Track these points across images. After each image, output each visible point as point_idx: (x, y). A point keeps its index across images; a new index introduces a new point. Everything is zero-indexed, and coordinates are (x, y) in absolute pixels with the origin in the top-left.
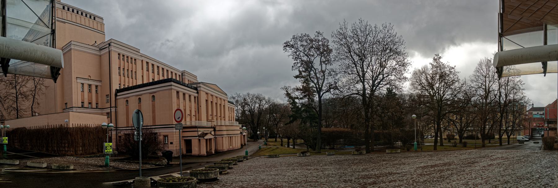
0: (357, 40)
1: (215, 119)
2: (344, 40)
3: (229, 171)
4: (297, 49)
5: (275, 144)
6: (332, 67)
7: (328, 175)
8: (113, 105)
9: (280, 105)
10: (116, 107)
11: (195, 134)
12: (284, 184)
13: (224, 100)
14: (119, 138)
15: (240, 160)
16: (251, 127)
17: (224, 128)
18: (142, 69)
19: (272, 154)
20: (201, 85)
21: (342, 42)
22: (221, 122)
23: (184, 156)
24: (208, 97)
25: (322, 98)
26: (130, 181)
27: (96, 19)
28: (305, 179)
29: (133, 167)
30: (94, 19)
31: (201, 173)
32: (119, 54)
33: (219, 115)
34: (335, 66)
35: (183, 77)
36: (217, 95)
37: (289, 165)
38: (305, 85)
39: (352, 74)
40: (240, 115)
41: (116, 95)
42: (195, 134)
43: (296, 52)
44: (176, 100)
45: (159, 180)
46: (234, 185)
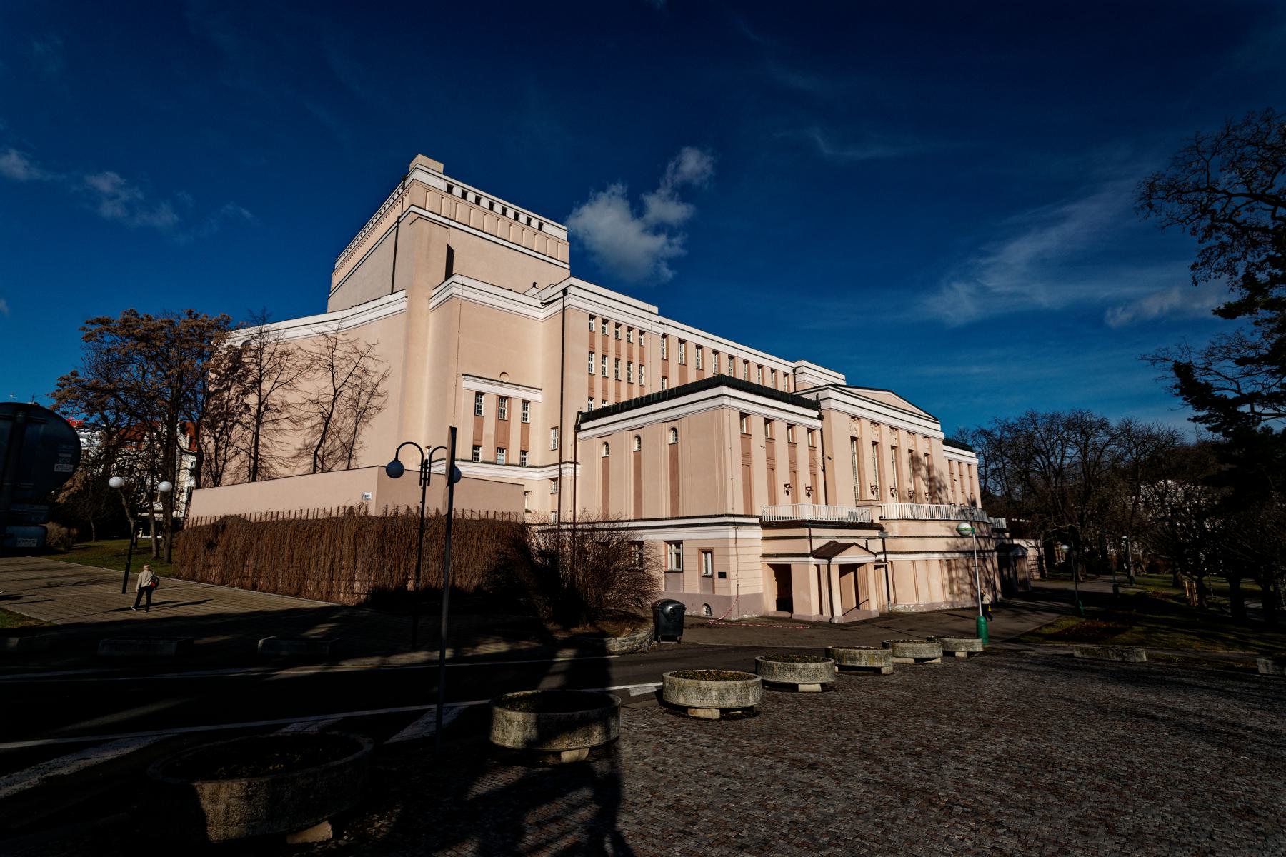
8: (568, 456)
20: (831, 393)
30: (540, 226)
41: (577, 429)
42: (804, 547)
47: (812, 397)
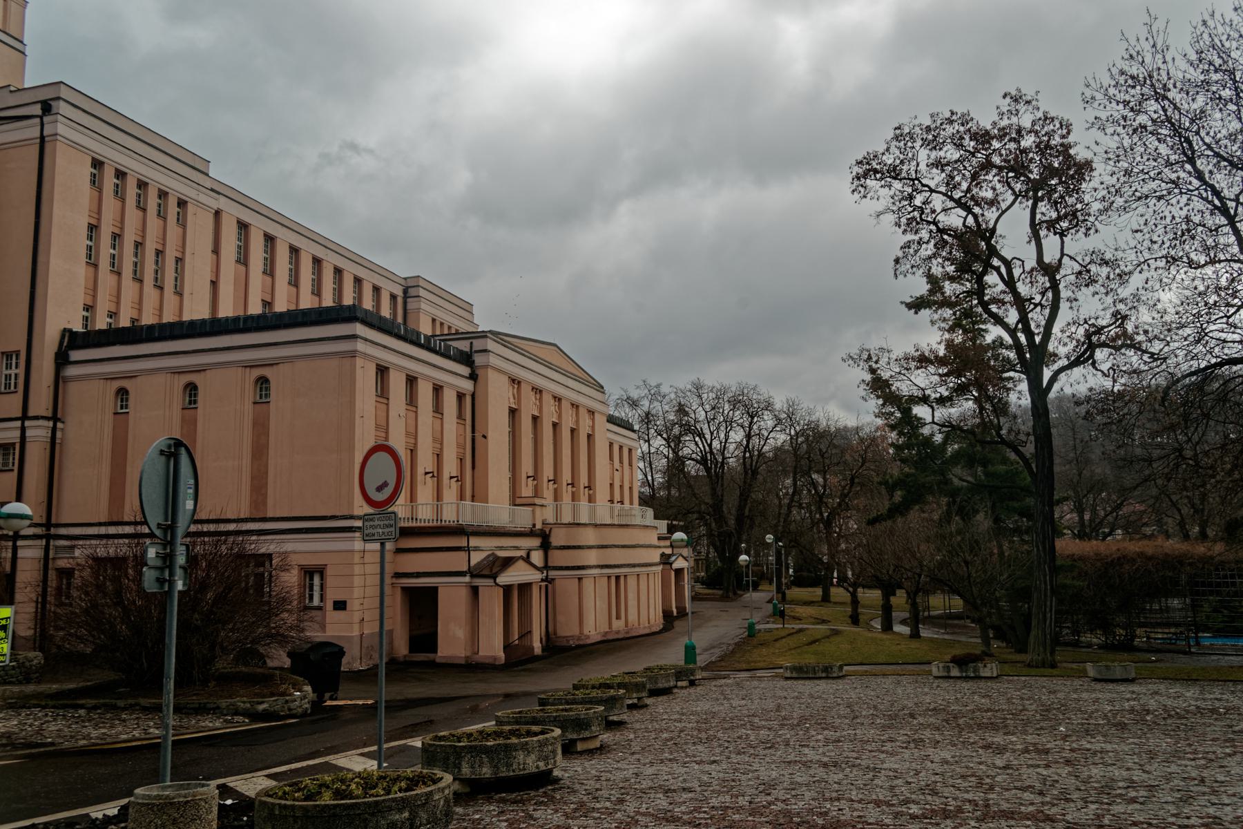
0: (1226, 93)
1: (548, 493)
2: (1152, 106)
3: (606, 737)
4: (914, 180)
5: (823, 612)
6: (1093, 242)
7: (1107, 787)
9: (843, 432)
10: (55, 418)
11: (457, 561)
12: (872, 814)
13: (591, 412)
14: (57, 582)
15: (662, 684)
16: (710, 535)
17: (590, 537)
18: (216, 251)
19: (809, 659)
20: (491, 345)
21: (1142, 119)
22: (575, 511)
23: (397, 669)
24: (518, 397)
25: (1052, 395)
26: (97, 812)
28: (978, 796)
29: (128, 730)
31: (476, 751)
32: (97, 164)
33: (566, 476)
34: (1113, 235)
35: (412, 304)
36: (560, 391)
37: (894, 719)
38: (958, 338)
39: (1213, 262)
40: (659, 479)
41: (62, 359)
42: (457, 561)
43: (911, 197)
44: (371, 403)
45: (267, 793)
46: (631, 807)
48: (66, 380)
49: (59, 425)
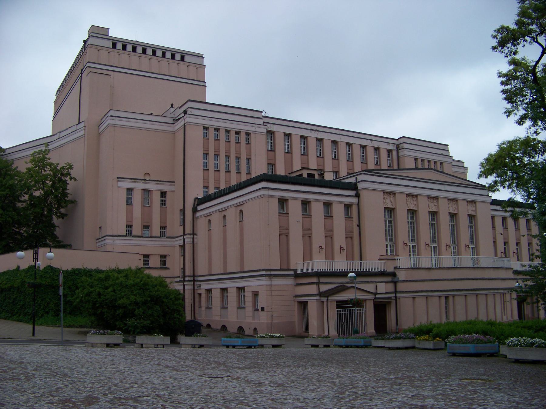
27: (187, 58)
30: (182, 58)
41: (195, 210)
47: (352, 180)
48: (197, 218)
49: (195, 236)
